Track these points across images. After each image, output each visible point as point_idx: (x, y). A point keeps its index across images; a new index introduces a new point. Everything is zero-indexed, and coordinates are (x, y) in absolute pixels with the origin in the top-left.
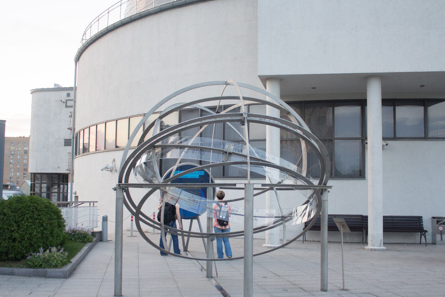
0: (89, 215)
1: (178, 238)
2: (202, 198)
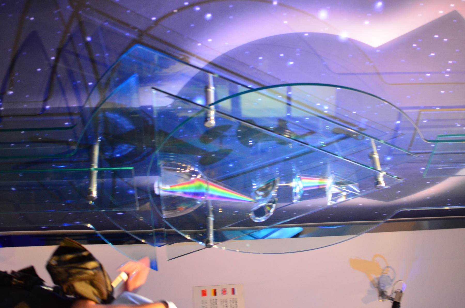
1: (299, 191)
2: (384, 300)
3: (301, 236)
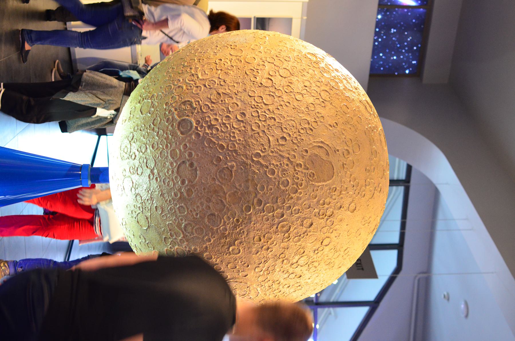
0: (399, 247)
3: (309, 225)
